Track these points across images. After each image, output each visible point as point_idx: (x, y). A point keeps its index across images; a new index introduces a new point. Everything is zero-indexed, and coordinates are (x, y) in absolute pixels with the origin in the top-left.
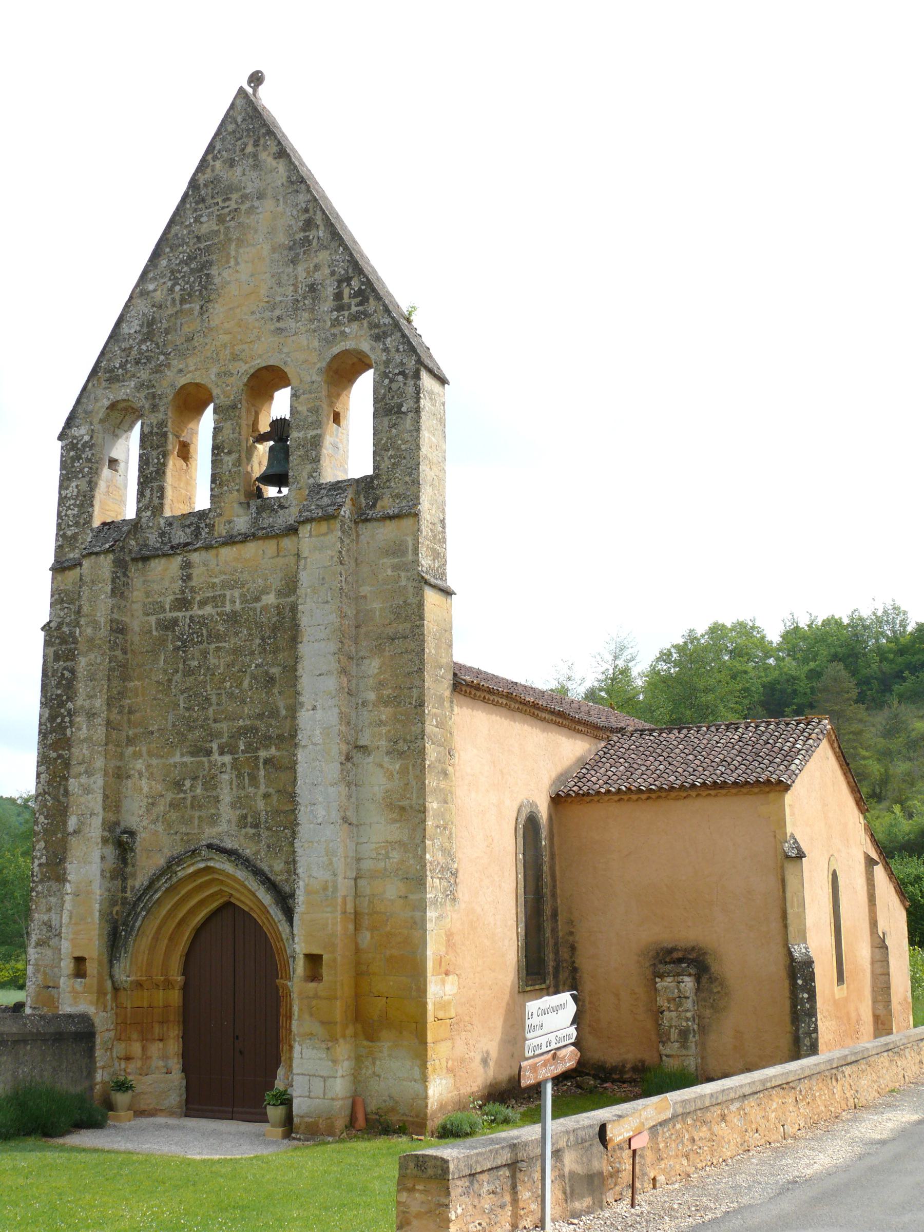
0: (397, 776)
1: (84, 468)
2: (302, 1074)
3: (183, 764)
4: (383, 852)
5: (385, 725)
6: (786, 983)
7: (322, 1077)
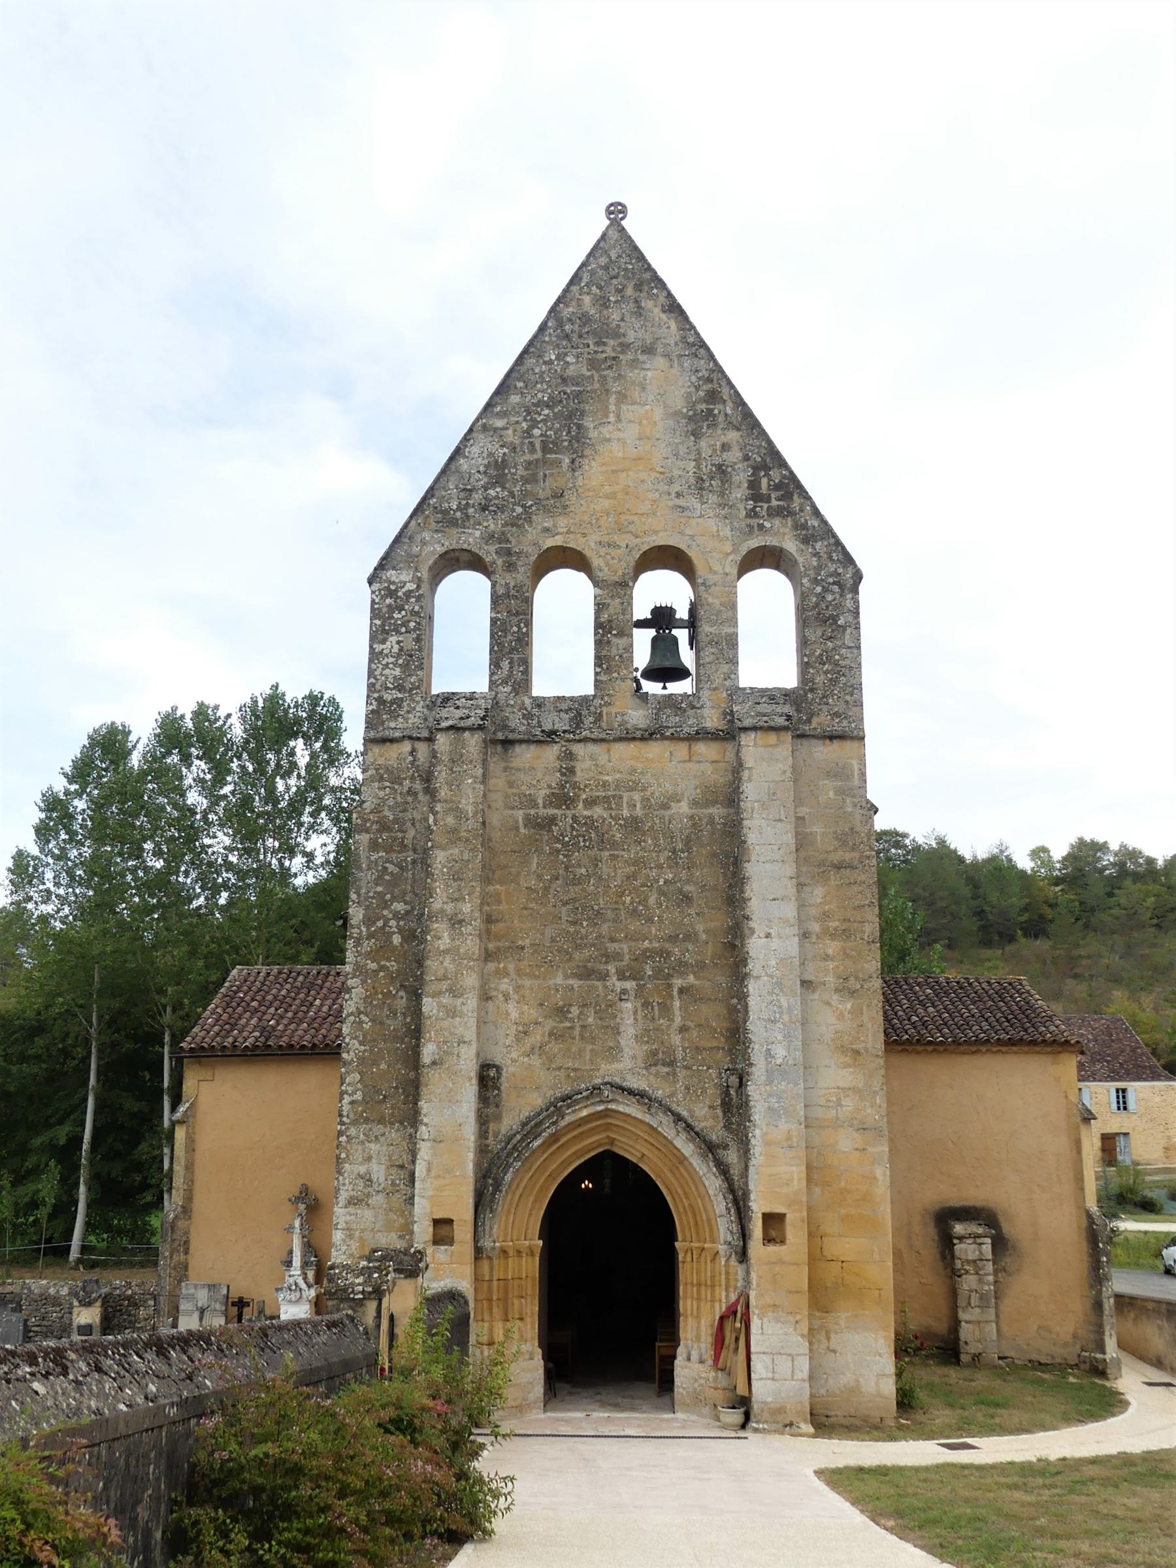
1: (409, 621)
2: (764, 1353)
3: (567, 987)
5: (832, 960)
6: (1084, 1246)
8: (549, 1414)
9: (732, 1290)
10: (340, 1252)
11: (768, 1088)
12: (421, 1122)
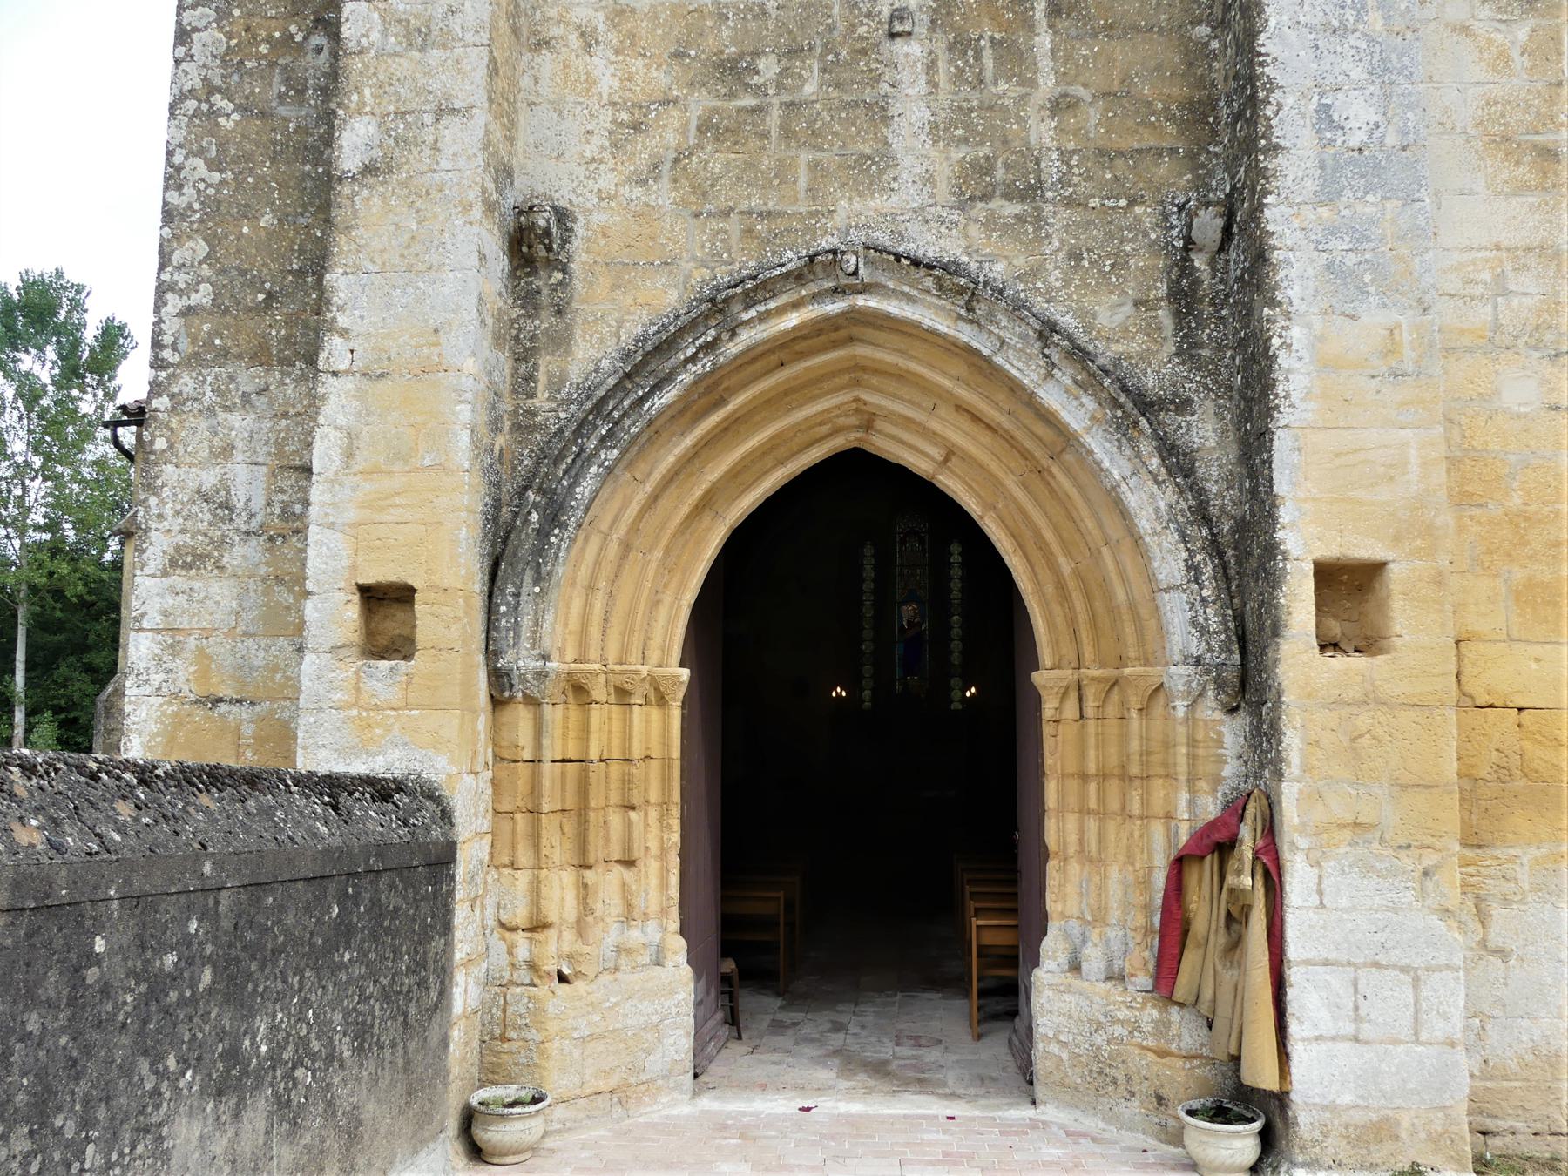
0: (1520, 62)
2: (1326, 963)
4: (1486, 276)
7: (1404, 969)
8: (707, 1103)
9: (1203, 785)
10: (147, 689)
11: (1324, 212)
12: (331, 327)
